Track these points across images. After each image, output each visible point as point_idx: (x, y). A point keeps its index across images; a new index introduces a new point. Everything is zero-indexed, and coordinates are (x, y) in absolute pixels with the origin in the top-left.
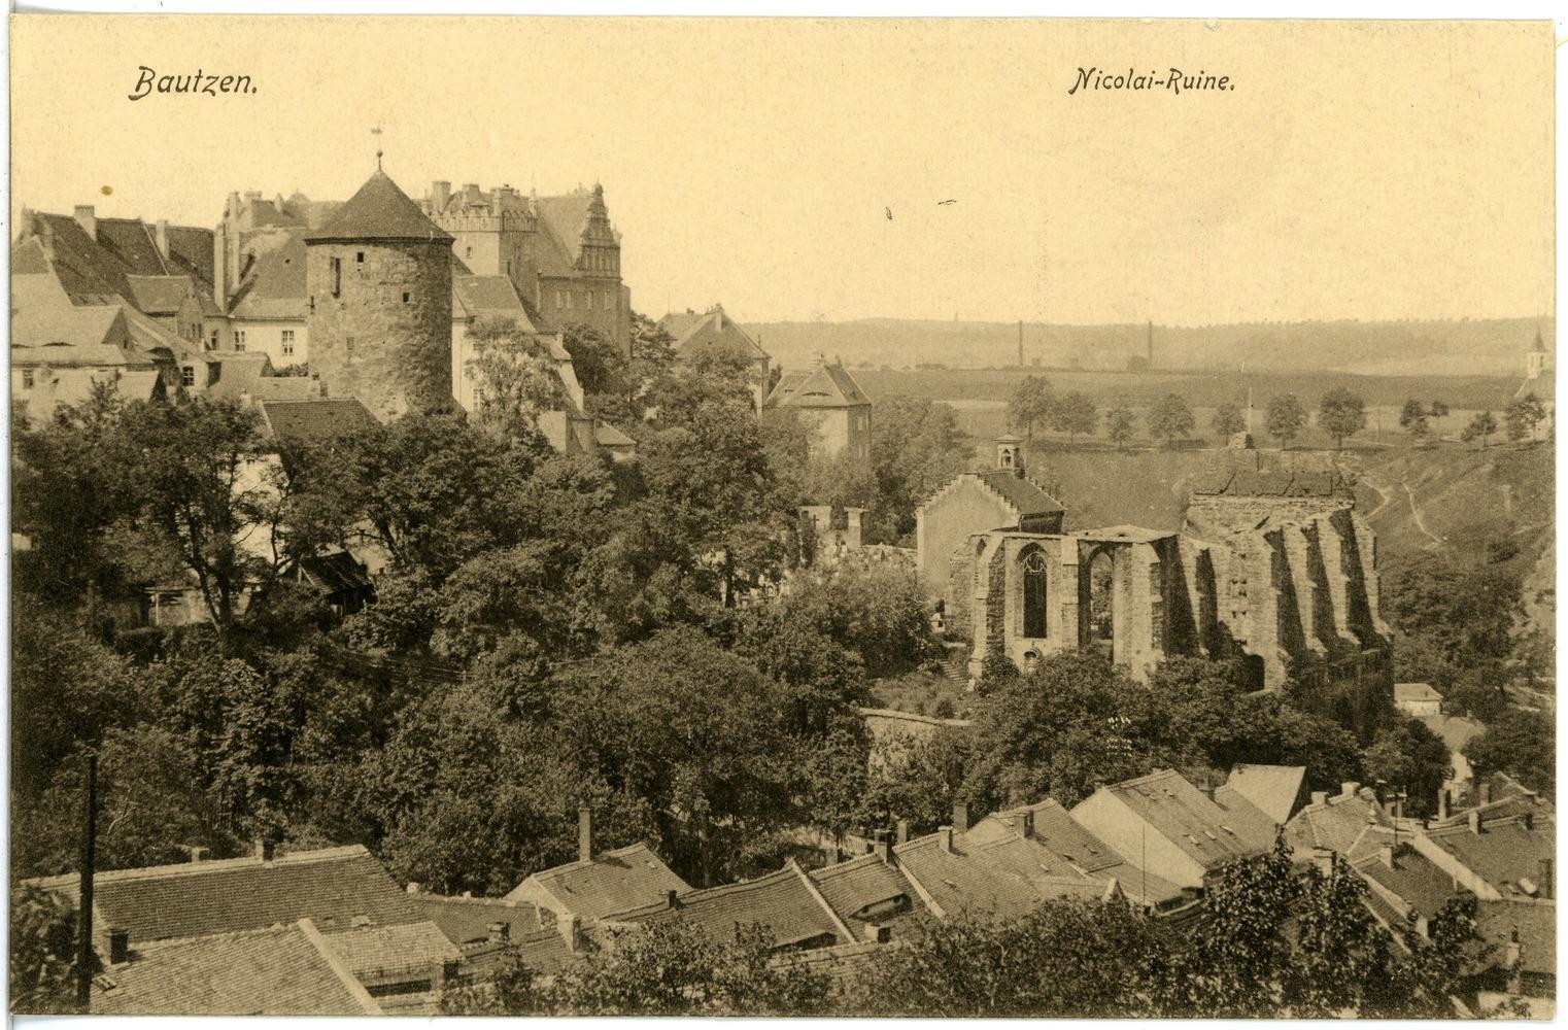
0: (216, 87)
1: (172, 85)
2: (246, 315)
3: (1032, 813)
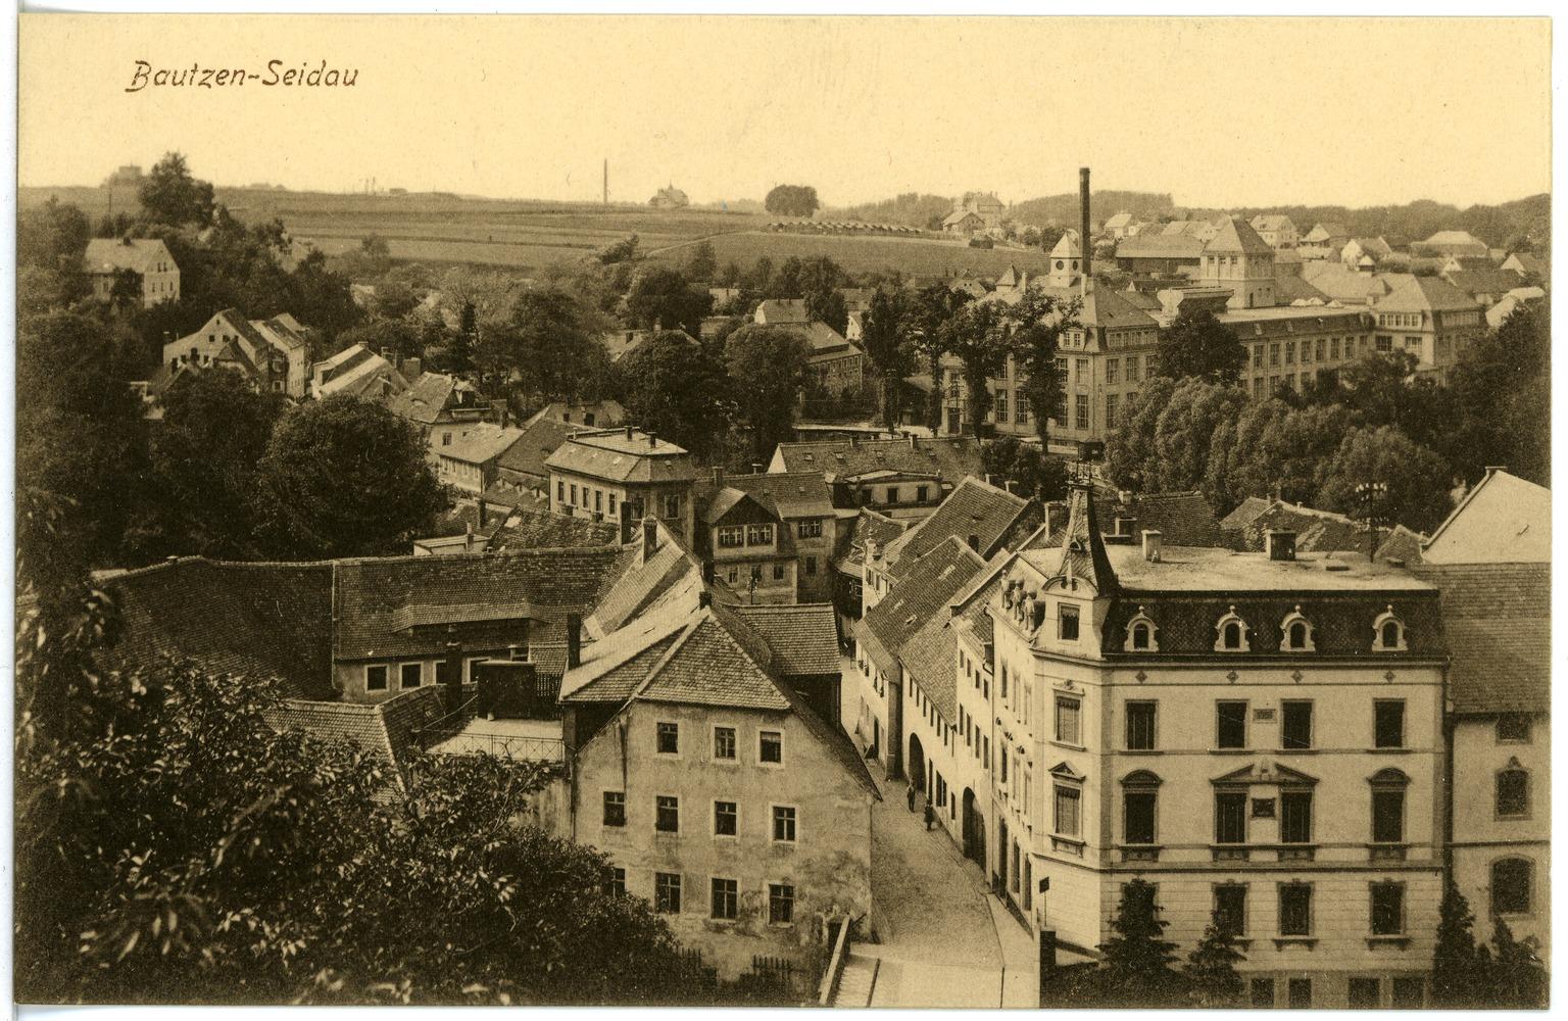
0: (212, 80)
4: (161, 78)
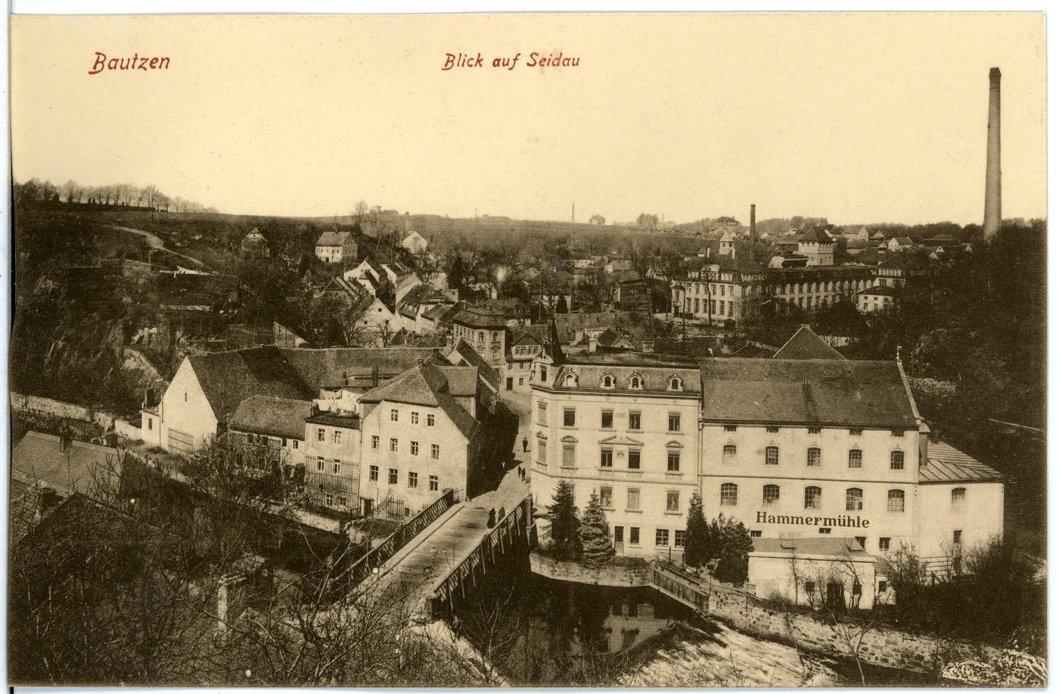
0: (147, 65)
1: (115, 64)
2: (322, 243)
3: (849, 507)
4: (566, 62)
